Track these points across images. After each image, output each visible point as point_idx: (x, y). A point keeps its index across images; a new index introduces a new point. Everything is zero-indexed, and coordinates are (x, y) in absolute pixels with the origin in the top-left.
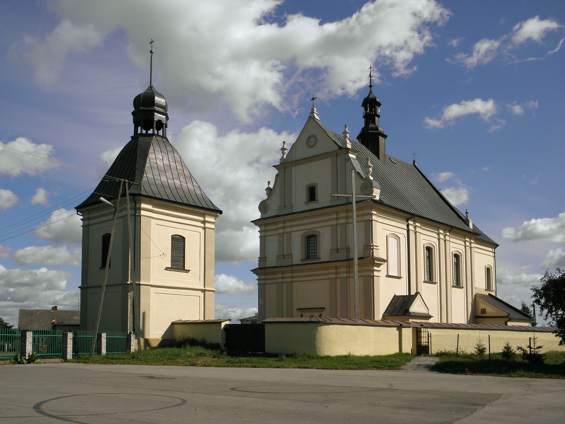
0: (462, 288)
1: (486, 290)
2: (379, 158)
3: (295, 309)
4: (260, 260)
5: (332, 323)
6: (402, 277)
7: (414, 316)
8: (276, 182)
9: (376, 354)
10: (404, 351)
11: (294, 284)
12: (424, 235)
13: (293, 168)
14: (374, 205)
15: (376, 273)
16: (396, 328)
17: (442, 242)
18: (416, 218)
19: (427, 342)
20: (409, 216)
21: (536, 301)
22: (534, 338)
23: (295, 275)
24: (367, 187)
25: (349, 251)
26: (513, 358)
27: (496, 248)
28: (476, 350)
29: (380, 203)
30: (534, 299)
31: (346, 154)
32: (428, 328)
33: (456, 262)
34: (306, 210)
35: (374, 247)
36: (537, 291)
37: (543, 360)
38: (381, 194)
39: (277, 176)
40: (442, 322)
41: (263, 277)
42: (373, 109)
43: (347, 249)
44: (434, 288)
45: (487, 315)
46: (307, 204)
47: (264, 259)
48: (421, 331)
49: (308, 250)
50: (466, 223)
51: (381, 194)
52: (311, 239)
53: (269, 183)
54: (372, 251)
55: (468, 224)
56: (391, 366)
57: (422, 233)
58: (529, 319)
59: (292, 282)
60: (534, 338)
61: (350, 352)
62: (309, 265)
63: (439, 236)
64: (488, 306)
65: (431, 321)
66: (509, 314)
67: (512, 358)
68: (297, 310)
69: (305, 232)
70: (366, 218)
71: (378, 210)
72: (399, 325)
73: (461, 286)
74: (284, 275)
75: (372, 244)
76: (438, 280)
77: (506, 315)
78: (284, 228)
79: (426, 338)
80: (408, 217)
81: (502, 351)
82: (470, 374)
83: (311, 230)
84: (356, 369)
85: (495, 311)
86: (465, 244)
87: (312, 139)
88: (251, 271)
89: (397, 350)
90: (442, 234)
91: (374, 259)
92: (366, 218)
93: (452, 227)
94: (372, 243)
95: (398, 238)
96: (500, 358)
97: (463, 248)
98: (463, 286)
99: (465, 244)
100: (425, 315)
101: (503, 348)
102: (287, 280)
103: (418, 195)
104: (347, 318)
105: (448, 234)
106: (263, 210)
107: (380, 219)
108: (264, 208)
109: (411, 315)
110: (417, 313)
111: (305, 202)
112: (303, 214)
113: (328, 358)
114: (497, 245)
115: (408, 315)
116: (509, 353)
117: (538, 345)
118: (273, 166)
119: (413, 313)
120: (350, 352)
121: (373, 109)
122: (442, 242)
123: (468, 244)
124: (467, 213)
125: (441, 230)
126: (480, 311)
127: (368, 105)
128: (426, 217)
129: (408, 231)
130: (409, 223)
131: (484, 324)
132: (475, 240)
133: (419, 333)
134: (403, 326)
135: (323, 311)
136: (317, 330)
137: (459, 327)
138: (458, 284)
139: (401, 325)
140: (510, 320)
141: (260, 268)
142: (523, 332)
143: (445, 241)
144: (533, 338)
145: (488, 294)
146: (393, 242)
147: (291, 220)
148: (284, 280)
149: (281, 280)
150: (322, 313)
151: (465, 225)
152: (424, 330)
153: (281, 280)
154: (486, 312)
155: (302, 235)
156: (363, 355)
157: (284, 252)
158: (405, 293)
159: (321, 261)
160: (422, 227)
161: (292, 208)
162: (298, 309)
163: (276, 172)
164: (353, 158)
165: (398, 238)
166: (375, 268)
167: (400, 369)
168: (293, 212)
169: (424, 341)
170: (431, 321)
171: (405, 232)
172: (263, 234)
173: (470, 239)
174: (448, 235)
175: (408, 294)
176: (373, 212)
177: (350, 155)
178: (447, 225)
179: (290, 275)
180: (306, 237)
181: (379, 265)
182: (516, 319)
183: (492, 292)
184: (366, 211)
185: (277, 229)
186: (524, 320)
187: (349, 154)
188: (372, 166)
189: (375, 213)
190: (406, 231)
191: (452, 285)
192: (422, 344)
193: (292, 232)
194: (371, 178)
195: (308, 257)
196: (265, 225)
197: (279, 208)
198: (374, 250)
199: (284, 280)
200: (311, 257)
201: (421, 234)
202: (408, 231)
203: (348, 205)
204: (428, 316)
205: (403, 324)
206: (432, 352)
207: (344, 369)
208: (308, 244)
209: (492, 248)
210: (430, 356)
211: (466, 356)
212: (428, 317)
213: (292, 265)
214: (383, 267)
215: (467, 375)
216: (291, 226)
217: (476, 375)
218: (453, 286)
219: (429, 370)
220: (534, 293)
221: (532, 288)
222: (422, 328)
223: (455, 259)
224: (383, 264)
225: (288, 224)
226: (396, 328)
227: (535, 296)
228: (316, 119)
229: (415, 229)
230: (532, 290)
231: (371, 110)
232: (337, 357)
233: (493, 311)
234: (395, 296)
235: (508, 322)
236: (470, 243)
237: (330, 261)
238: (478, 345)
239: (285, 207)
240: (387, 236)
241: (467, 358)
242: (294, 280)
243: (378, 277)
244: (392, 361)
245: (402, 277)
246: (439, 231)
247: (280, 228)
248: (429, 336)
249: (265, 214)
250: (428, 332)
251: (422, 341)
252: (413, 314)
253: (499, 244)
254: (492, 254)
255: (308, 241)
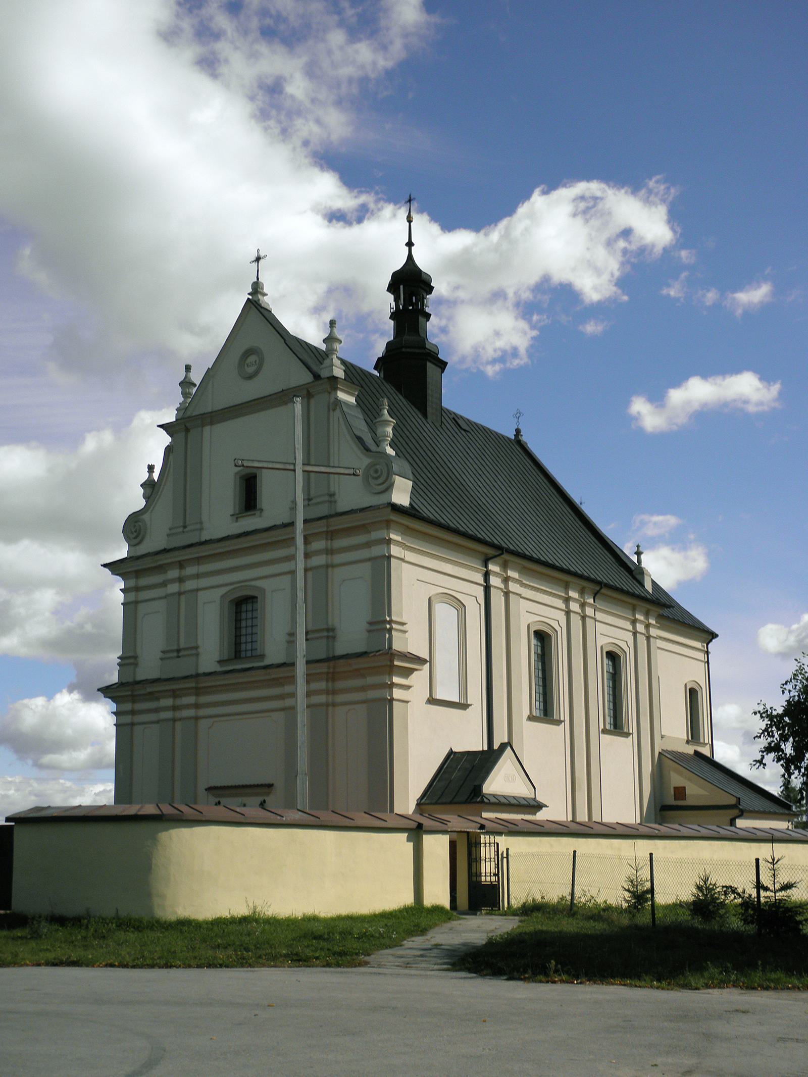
0: (627, 735)
1: (688, 742)
2: (425, 415)
3: (202, 785)
4: (123, 662)
5: (204, 819)
6: (471, 705)
7: (494, 804)
8: (167, 464)
9: (344, 911)
10: (428, 902)
11: (203, 724)
12: (544, 607)
13: (207, 429)
14: (394, 517)
15: (397, 693)
16: (406, 835)
17: (576, 621)
18: (506, 556)
19: (495, 875)
20: (490, 551)
21: (768, 749)
22: (773, 860)
23: (204, 699)
24: (378, 474)
25: (334, 637)
26: (721, 917)
27: (711, 641)
28: (627, 895)
29: (409, 512)
30: (763, 742)
31: (330, 393)
32: (500, 834)
33: (611, 670)
34: (232, 535)
35: (394, 626)
36: (771, 717)
37: (800, 922)
38: (415, 492)
39: (168, 450)
40: (593, 820)
41: (128, 706)
42: (414, 298)
43: (328, 630)
44: (556, 734)
45: (689, 802)
46: (237, 518)
47: (132, 661)
48: (480, 844)
49: (238, 636)
50: (638, 577)
51: (414, 492)
52: (244, 608)
53: (151, 468)
54: (387, 636)
55: (641, 581)
56: (342, 954)
57: (523, 596)
58: (787, 812)
59: (197, 718)
60: (773, 860)
61: (255, 908)
62: (237, 675)
63: (568, 606)
64: (690, 780)
65: (541, 816)
66: (739, 799)
67: (717, 919)
68: (206, 790)
69: (230, 591)
70: (376, 551)
71: (407, 531)
72: (414, 825)
73: (625, 730)
74: (179, 702)
75: (388, 619)
76: (564, 715)
77: (733, 801)
78: (181, 580)
79: (493, 864)
80: (486, 554)
81: (692, 898)
82: (562, 981)
83: (243, 584)
84: (227, 966)
85: (707, 793)
86: (634, 627)
87: (252, 359)
88: (99, 690)
89: (408, 899)
90: (575, 600)
91: (391, 654)
92: (376, 551)
93: (599, 583)
94: (390, 615)
95: (461, 607)
96: (685, 916)
97: (629, 637)
98: (631, 731)
99: (634, 627)
100: (506, 801)
101: (695, 891)
102: (186, 713)
103: (518, 506)
104: (327, 809)
105: (591, 601)
106: (134, 536)
107: (410, 556)
108: (136, 532)
109: (486, 800)
110: (504, 797)
111: (232, 515)
112: (228, 543)
113: (184, 925)
114: (714, 636)
115: (479, 802)
116: (709, 904)
117: (783, 879)
118: (159, 426)
119: (494, 796)
120: (255, 908)
121: (414, 298)
122: (576, 621)
123: (640, 628)
124: (639, 554)
125: (571, 591)
126: (672, 792)
127: (401, 287)
128: (540, 559)
129: (487, 589)
130: (489, 568)
131: (699, 825)
132: (660, 617)
133: (474, 849)
134: (424, 829)
135: (268, 794)
136: (155, 840)
137: (591, 831)
138: (617, 726)
139: (420, 826)
140: (742, 814)
141: (121, 685)
142: (762, 845)
143: (584, 618)
144: (771, 861)
145: (692, 752)
146: (445, 615)
147: (199, 560)
148: (178, 714)
149: (169, 715)
150: (266, 799)
151: (635, 582)
152: (487, 841)
153: (169, 715)
154: (685, 795)
155: (223, 597)
156: (299, 914)
157: (178, 640)
158: (477, 743)
159: (267, 662)
160: (524, 582)
161: (201, 529)
162: (209, 789)
163: (167, 440)
164: (347, 404)
165: (461, 607)
166: (396, 680)
167: (360, 965)
168: (203, 540)
169: (488, 871)
170: (541, 816)
171: (480, 592)
172: (132, 596)
173: (647, 614)
174: (590, 605)
175: (486, 748)
176: (393, 536)
177: (341, 395)
178: (588, 579)
179: (191, 700)
180: (231, 601)
181: (407, 673)
182: (757, 812)
183: (703, 748)
184: (375, 535)
185: (164, 584)
186: (775, 813)
187: (338, 392)
188: (394, 422)
189: (399, 538)
190: (482, 588)
191: (602, 727)
192: (483, 879)
193: (197, 590)
194: (390, 451)
195: (237, 653)
196: (138, 574)
197: (170, 529)
198: (394, 633)
199: (178, 714)
200: (243, 654)
201: (521, 599)
202: (487, 589)
203: (331, 520)
204: (533, 803)
205: (427, 823)
206: (513, 902)
207: (190, 966)
208: (238, 620)
209: (702, 642)
210: (505, 914)
211: (603, 913)
212: (537, 806)
213: (198, 675)
214: (419, 679)
215: (554, 982)
216: (198, 576)
217: (581, 983)
218: (605, 731)
219: (449, 966)
220: (763, 724)
221: (758, 708)
222: (483, 833)
223: (610, 663)
224: (416, 670)
225: (190, 570)
226: (406, 835)
227: (767, 731)
228: (262, 307)
229: (507, 586)
230: (758, 715)
231: (408, 301)
232: (219, 923)
233: (702, 792)
234: (451, 752)
235: (737, 820)
236: (648, 626)
237: (287, 662)
238: (632, 881)
239: (185, 527)
240: (430, 599)
241: (595, 920)
242: (202, 712)
243: (406, 704)
244: (365, 933)
245: (471, 705)
246: (567, 593)
247: (172, 581)
248: (502, 859)
249: (137, 547)
250: (498, 844)
251: (483, 871)
252: (493, 800)
253: (717, 633)
254: (701, 656)
255: (238, 612)
